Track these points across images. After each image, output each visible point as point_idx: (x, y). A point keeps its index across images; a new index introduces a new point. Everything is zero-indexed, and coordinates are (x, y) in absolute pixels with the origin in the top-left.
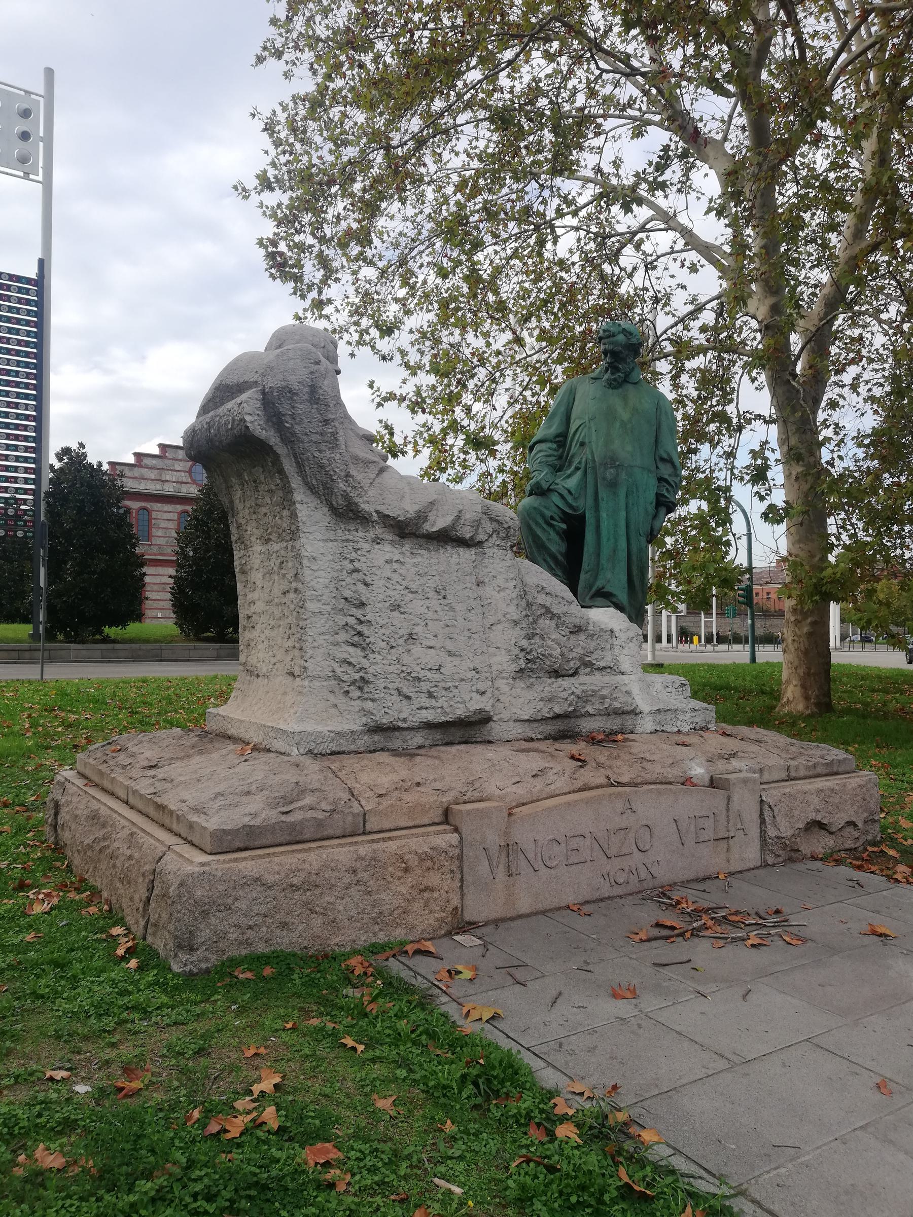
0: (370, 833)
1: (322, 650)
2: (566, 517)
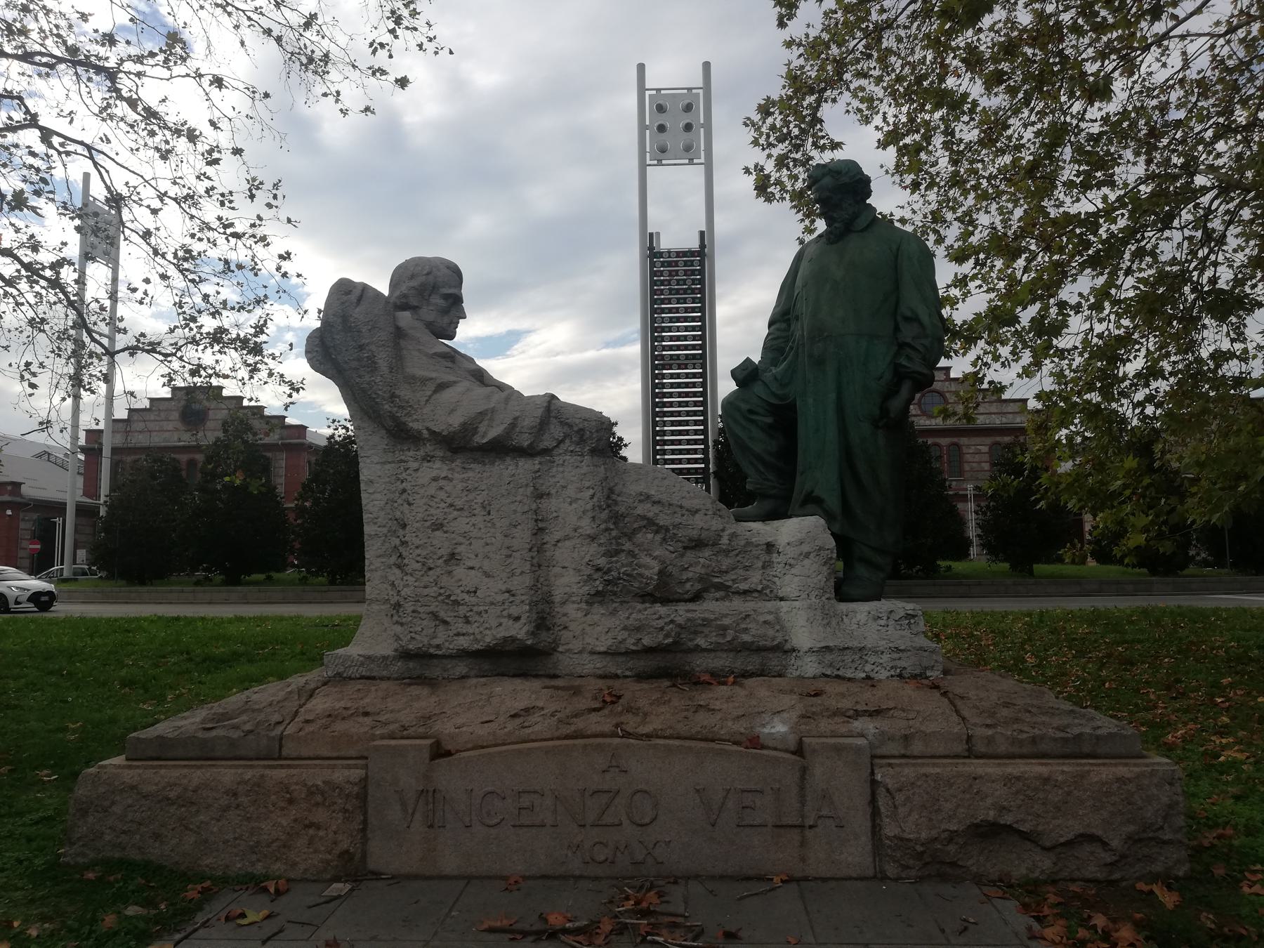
0: (286, 759)
1: (379, 573)
2: (774, 410)
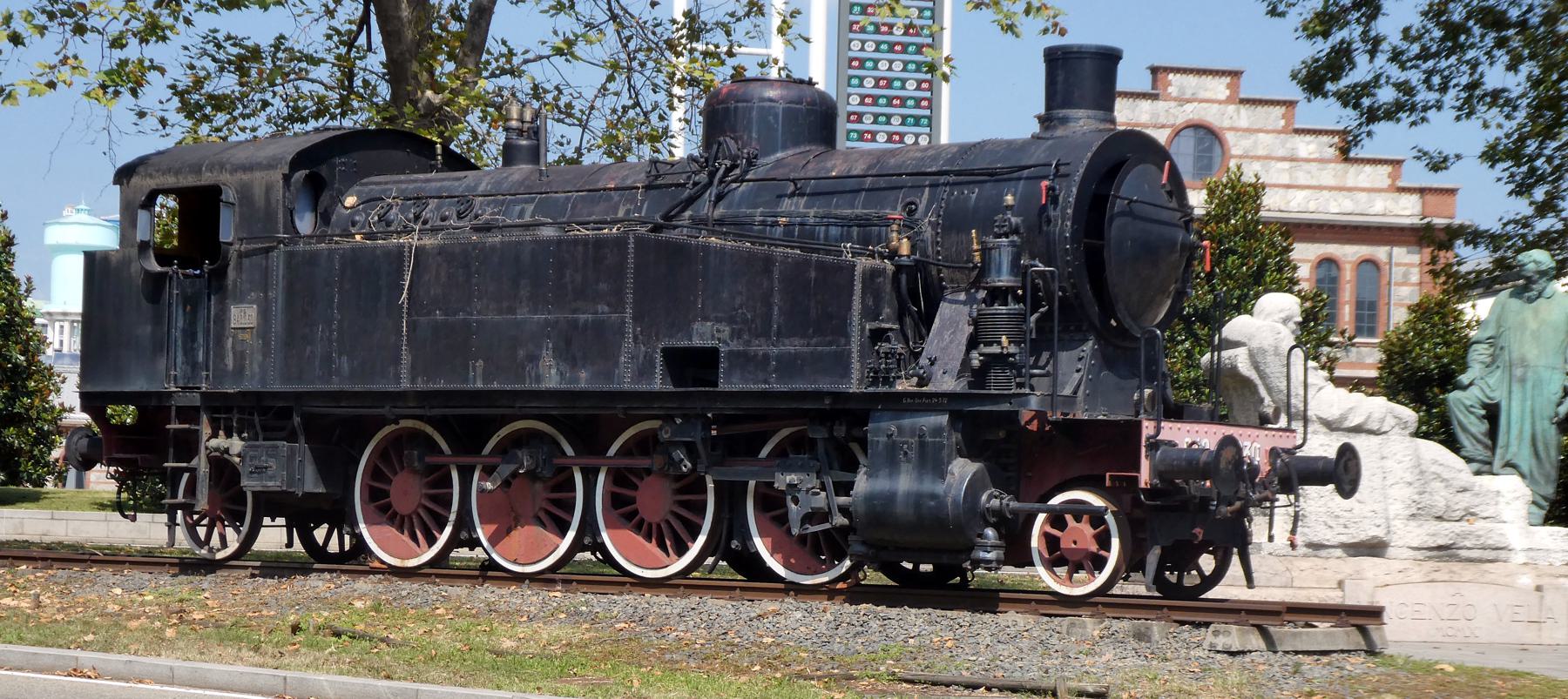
2: (1485, 406)
